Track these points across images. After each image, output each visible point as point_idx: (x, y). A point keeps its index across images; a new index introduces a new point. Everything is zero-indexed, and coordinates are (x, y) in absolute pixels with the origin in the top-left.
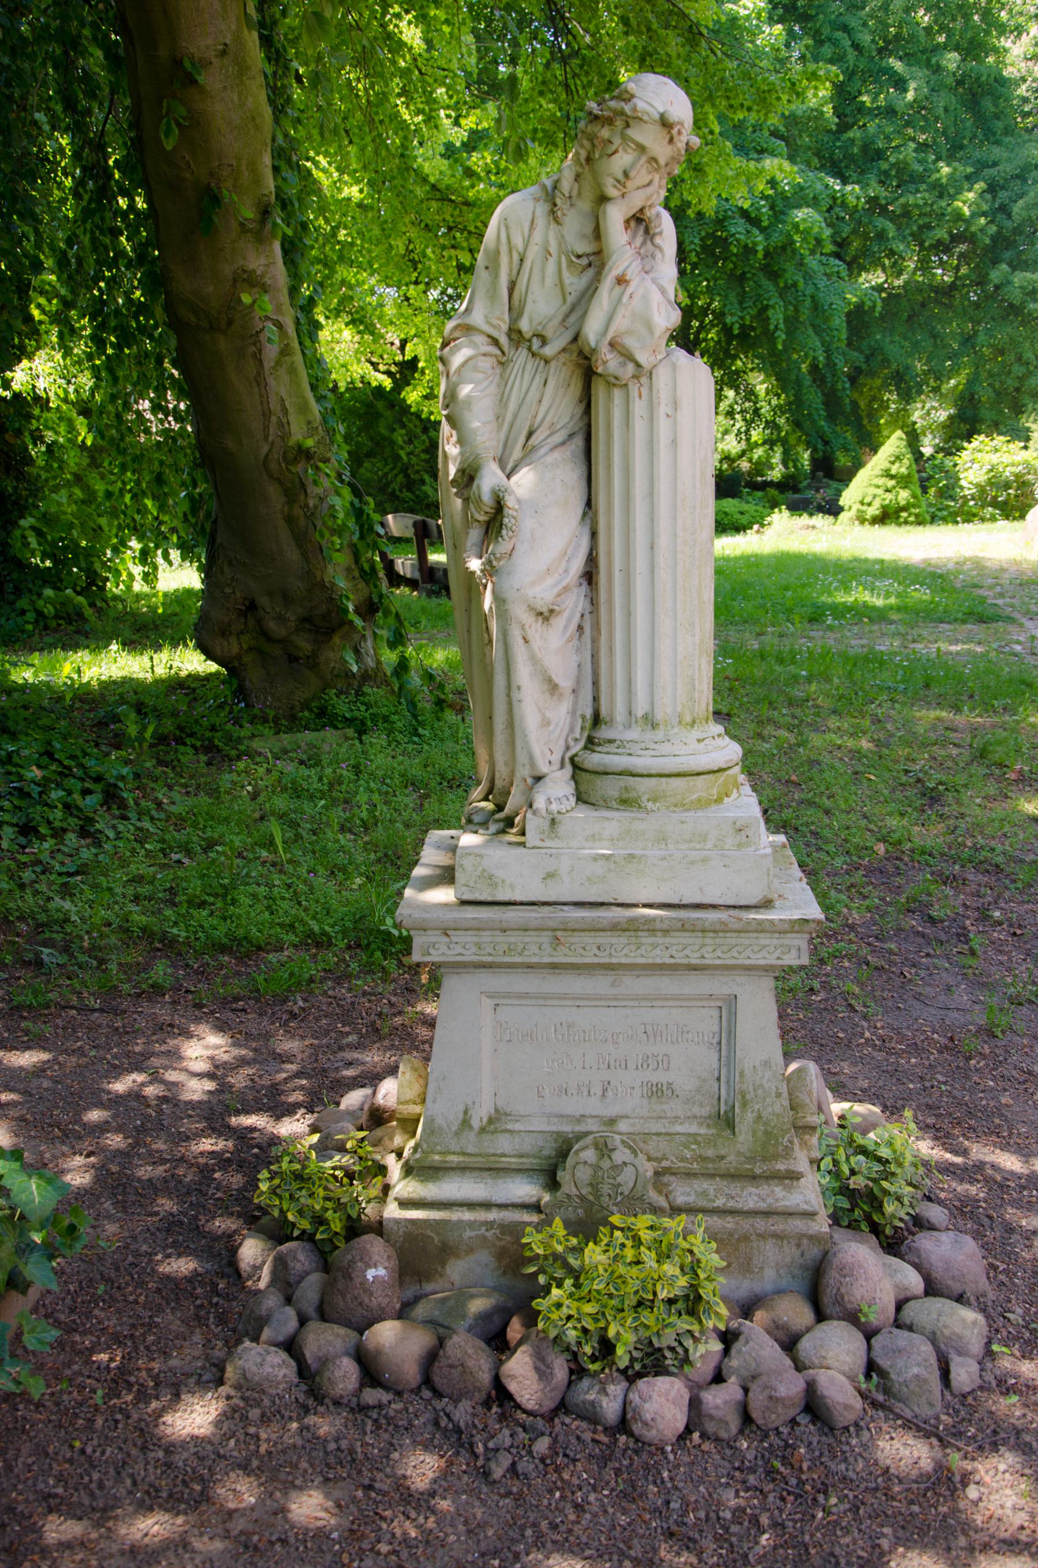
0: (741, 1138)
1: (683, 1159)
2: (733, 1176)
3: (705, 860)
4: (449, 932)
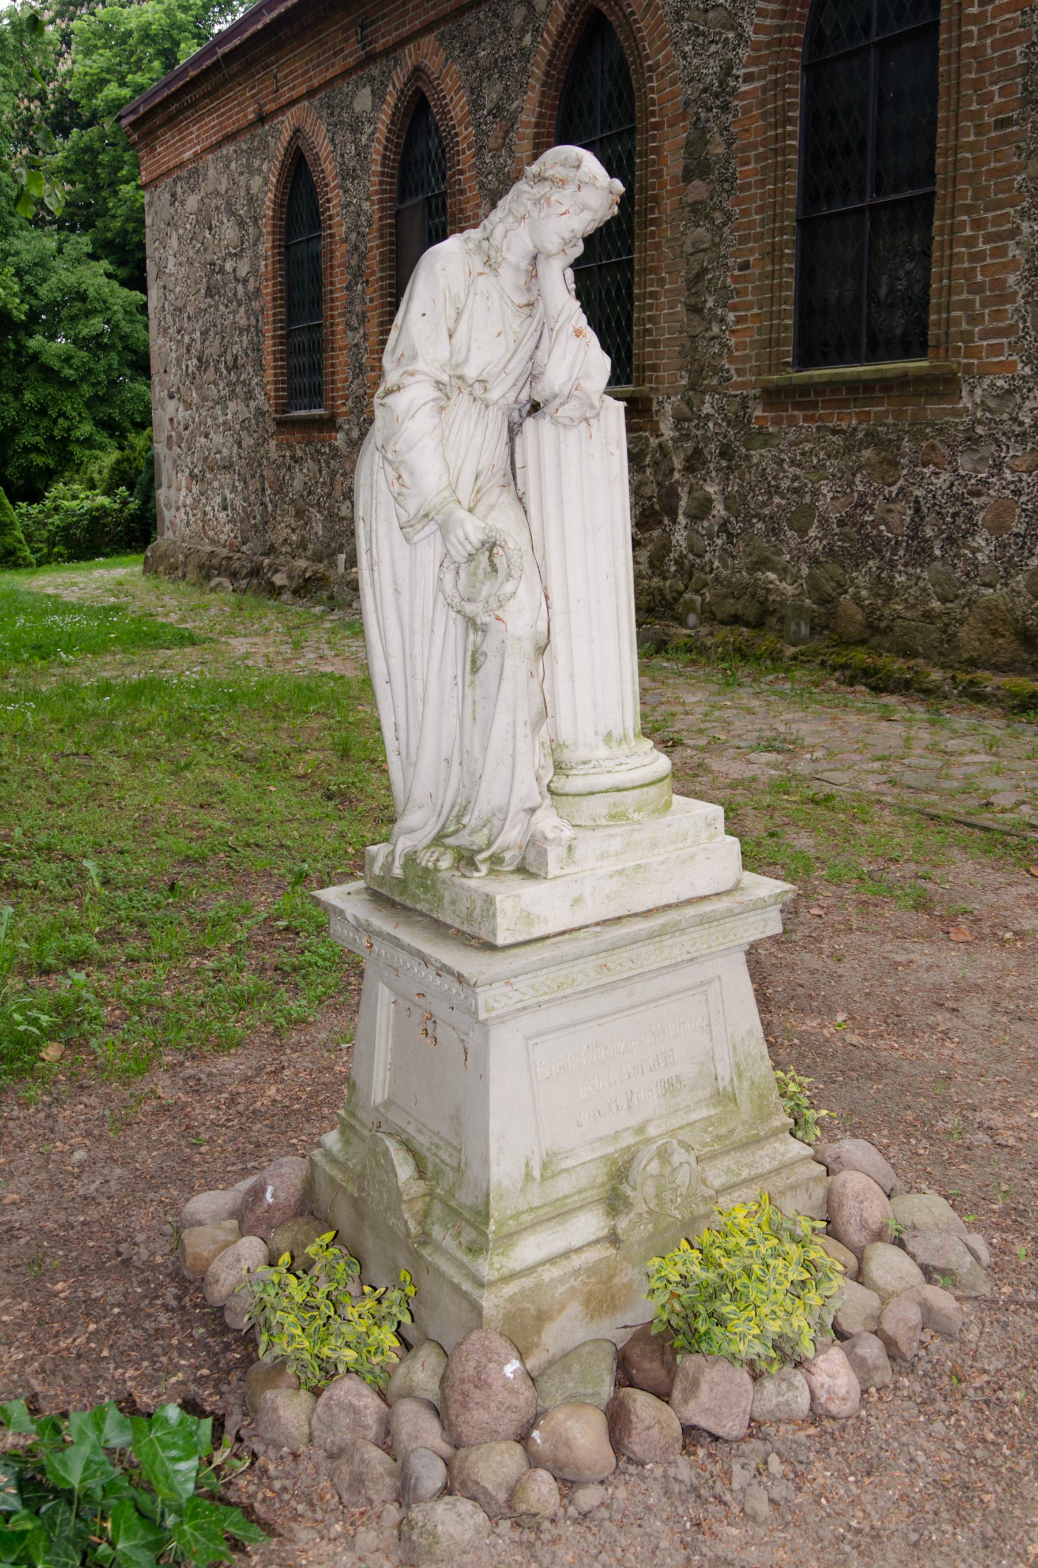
0: (743, 1108)
1: (705, 1145)
2: (743, 1146)
3: (692, 857)
4: (512, 980)
